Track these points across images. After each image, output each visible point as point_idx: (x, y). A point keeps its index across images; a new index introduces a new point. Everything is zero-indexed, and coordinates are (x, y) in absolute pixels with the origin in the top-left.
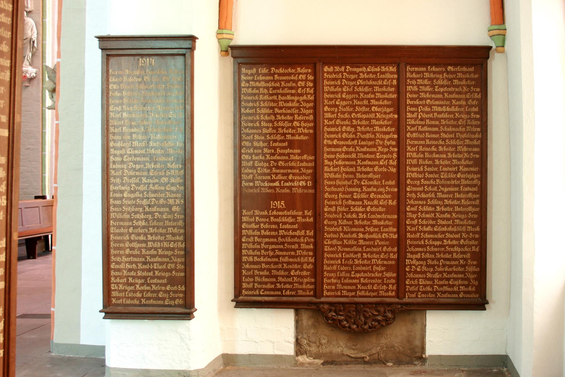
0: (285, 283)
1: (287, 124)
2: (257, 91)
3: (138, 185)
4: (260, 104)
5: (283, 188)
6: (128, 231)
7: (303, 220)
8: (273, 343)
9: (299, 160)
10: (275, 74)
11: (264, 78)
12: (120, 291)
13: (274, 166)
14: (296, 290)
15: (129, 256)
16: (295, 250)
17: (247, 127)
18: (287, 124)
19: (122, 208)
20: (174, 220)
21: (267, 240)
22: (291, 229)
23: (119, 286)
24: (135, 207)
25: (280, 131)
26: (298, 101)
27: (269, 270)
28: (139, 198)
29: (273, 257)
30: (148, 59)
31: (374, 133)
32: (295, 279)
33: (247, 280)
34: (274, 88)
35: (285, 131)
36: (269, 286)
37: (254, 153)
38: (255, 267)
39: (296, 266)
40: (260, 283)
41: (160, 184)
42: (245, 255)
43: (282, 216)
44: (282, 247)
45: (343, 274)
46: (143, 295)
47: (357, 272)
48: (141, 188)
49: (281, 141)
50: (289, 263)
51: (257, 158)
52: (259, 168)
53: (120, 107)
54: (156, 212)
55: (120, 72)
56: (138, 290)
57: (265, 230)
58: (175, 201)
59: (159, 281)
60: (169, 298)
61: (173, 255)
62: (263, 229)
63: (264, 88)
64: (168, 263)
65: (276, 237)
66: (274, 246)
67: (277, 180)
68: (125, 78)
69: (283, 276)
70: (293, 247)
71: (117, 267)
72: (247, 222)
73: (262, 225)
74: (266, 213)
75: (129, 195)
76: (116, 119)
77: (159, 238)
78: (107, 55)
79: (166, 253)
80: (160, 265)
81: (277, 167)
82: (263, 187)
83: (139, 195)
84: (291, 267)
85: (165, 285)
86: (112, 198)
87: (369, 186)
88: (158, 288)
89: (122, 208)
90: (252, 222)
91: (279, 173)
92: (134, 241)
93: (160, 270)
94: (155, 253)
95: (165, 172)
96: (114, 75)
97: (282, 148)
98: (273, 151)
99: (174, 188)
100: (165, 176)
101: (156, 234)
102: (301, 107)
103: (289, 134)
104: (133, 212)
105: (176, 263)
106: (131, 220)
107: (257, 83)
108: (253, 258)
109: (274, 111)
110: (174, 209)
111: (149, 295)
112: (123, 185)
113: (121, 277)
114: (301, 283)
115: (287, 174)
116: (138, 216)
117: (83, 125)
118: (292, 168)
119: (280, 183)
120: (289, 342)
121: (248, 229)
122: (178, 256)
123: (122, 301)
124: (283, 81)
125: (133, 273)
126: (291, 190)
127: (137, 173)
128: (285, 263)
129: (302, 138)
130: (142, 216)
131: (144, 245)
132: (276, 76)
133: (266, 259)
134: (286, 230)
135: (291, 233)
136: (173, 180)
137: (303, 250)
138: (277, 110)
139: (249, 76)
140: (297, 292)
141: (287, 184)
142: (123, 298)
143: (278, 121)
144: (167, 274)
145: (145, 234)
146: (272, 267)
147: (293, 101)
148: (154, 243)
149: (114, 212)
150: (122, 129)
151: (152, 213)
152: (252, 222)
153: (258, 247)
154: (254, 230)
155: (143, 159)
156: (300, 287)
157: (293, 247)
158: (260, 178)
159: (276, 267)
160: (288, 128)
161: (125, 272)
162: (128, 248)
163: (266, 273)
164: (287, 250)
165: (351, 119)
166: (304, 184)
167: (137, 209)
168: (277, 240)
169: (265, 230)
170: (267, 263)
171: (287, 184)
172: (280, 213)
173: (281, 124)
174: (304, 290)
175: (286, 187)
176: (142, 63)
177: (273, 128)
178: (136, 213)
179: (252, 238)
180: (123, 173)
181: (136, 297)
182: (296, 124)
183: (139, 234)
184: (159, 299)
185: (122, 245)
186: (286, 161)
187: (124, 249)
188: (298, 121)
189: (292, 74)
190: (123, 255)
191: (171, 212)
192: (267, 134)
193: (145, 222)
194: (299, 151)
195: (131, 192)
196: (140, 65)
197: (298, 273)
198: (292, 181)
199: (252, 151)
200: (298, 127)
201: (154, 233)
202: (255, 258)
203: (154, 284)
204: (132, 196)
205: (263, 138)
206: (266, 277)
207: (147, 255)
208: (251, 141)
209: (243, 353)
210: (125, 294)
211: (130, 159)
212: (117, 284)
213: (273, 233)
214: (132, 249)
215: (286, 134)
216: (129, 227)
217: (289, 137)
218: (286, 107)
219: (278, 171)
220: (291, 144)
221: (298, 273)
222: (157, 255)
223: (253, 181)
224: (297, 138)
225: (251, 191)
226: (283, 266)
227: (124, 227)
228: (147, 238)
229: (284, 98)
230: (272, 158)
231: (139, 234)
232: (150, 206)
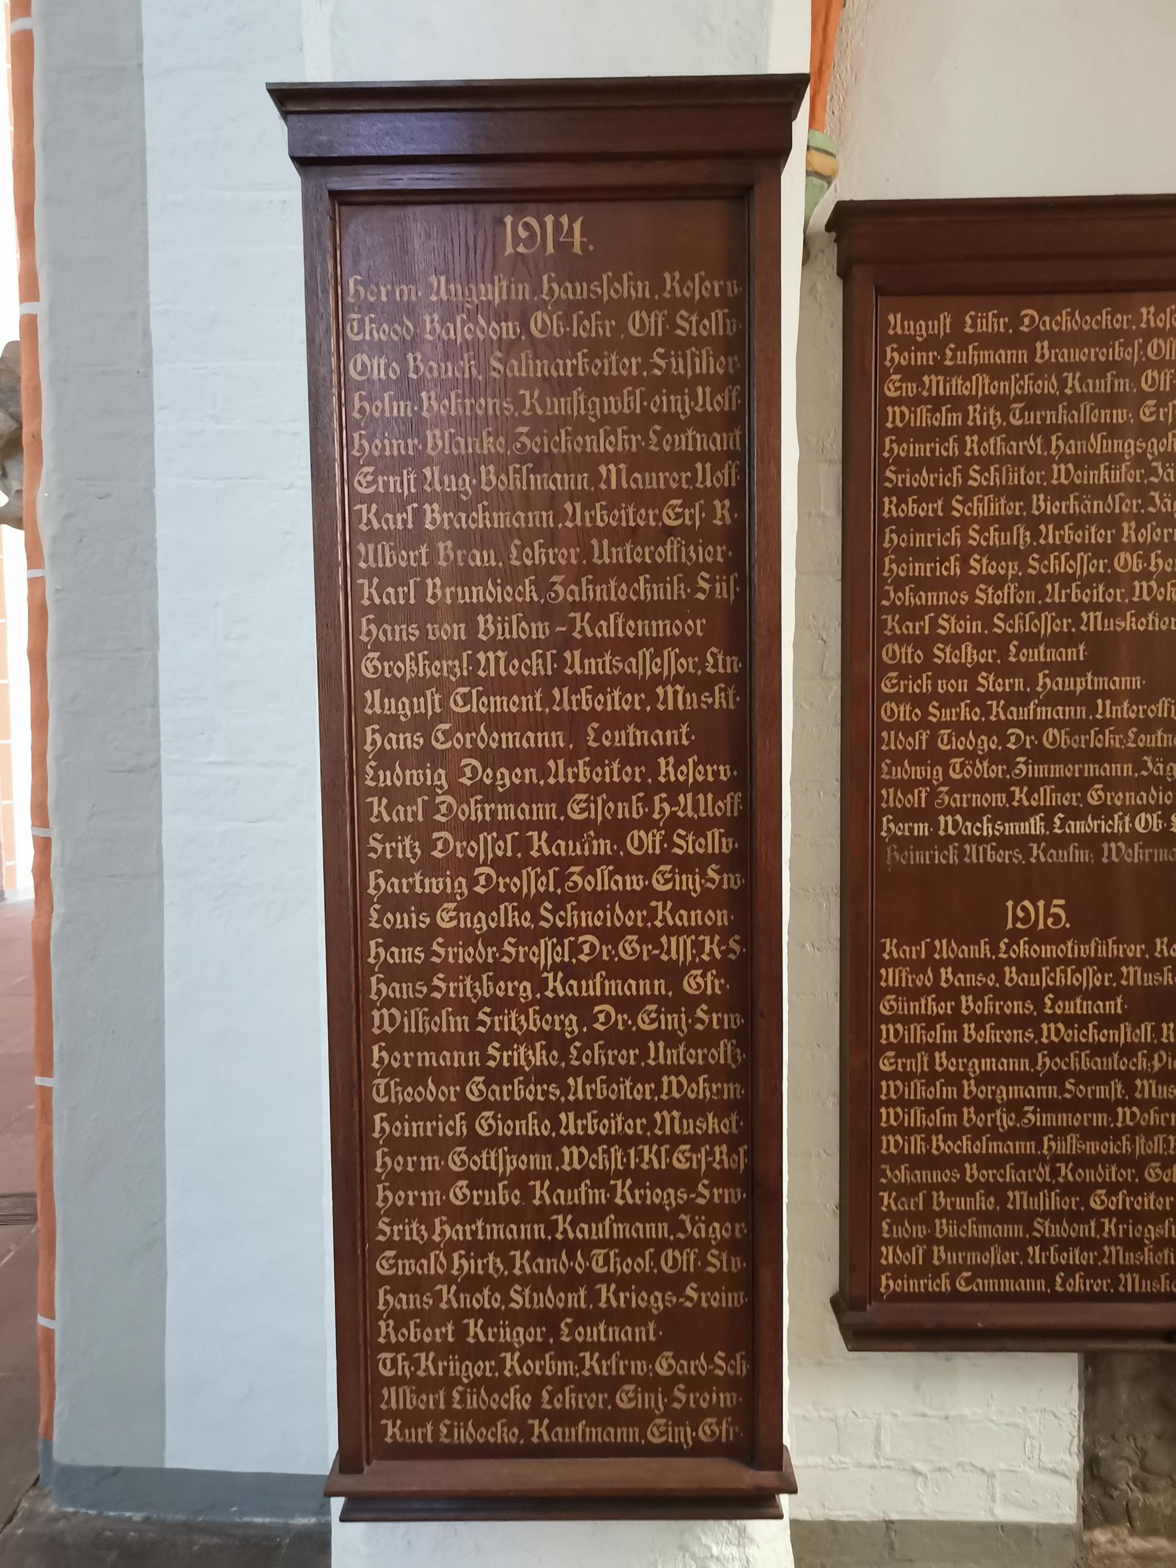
0: (1065, 1244)
1: (1083, 565)
2: (955, 419)
4: (966, 477)
5: (1059, 842)
6: (461, 1095)
7: (1149, 980)
8: (991, 1475)
9: (1137, 722)
10: (1036, 334)
11: (986, 357)
12: (423, 1386)
13: (1022, 751)
14: (1112, 1272)
15: (467, 1214)
16: (1108, 1107)
17: (909, 579)
18: (1083, 565)
19: (428, 983)
20: (696, 1040)
21: (988, 1064)
22: (1093, 1017)
23: (416, 1363)
24: (494, 980)
25: (1056, 594)
26: (1140, 461)
27: (997, 1190)
28: (515, 931)
29: (1013, 1134)
30: (549, 220)
32: (1109, 1225)
33: (900, 1233)
34: (1033, 403)
35: (1076, 595)
36: (994, 1257)
37: (934, 695)
38: (937, 1177)
39: (1112, 1174)
40: (952, 1244)
41: (623, 864)
42: (891, 1130)
43: (1055, 962)
44: (1052, 1092)
46: (536, 1401)
48: (530, 882)
49: (1055, 641)
50: (1081, 1161)
51: (948, 715)
52: (957, 761)
53: (409, 475)
54: (603, 999)
55: (404, 292)
56: (515, 1379)
57: (980, 1021)
58: (698, 946)
59: (616, 1334)
60: (668, 1413)
61: (690, 1207)
62: (972, 1017)
63: (987, 401)
64: (661, 1245)
65: (1028, 1051)
66: (1016, 1092)
67: (1033, 811)
68: (431, 323)
69: (1055, 1217)
70: (1102, 1092)
71: (408, 1267)
72: (899, 992)
73: (966, 1001)
74: (983, 950)
75: (465, 920)
76: (388, 535)
77: (617, 1124)
78: (333, 194)
79: (655, 1197)
80: (622, 1256)
81: (1038, 755)
82: (972, 839)
83: (514, 920)
84: (1089, 1175)
85: (649, 1352)
86: (374, 934)
88: (616, 1365)
89: (428, 983)
90: (925, 991)
91: (1045, 781)
92: (494, 1142)
93: (623, 1283)
94: (599, 1196)
95: (648, 802)
96: (371, 307)
98: (1019, 684)
99: (691, 883)
100: (647, 823)
101: (605, 1108)
102: (1154, 487)
103: (1092, 607)
104: (484, 1002)
105: (703, 1245)
106: (473, 1041)
107: (957, 381)
108: (928, 1141)
109: (1028, 506)
110: (690, 984)
111: (569, 1399)
112: (431, 868)
113: (428, 1319)
114: (1136, 1245)
115: (1082, 785)
116: (510, 1021)
117: (153, 584)
118: (1102, 756)
119: (1049, 825)
120: (1055, 1472)
121: (906, 1020)
122: (712, 1212)
123: (436, 1432)
124: (1071, 367)
125: (485, 1299)
126: (1099, 853)
127: (506, 812)
128: (1066, 1159)
130: (533, 1022)
131: (540, 1161)
132: (1043, 348)
133: (986, 1146)
134: (1069, 1020)
135: (1091, 1034)
136: (685, 844)
137: (1145, 1105)
138: (1040, 503)
139: (921, 347)
140: (1116, 1282)
141: (1078, 827)
142: (436, 1416)
143: (1044, 552)
145: (549, 1110)
146: (1010, 1175)
147: (1114, 459)
148: (592, 1150)
149: (388, 1003)
150: (421, 589)
151: (583, 1007)
152: (925, 991)
153: (950, 1092)
154: (930, 1022)
155: (532, 740)
156: (1131, 1259)
157: (1102, 1092)
158: (960, 800)
159: (1025, 1176)
160: (1088, 582)
161: (447, 1293)
162: (460, 1176)
163: (982, 1202)
164: (1075, 1106)
166: (1156, 824)
167: (504, 989)
168: (1033, 1063)
169: (980, 1021)
170: (985, 1161)
171: (1078, 827)
172: (1048, 951)
173: (1057, 564)
174: (1147, 1272)
175: (1076, 837)
176: (516, 239)
177: (1024, 582)
178: (499, 1005)
179: (923, 1057)
180: (431, 808)
181: (501, 1413)
182: (1126, 561)
183: (514, 1110)
184: (616, 1417)
185: (430, 1163)
186: (1076, 727)
188: (1134, 548)
189: (1114, 334)
190: (436, 1211)
191: (678, 1001)
192: (994, 609)
193: (548, 1049)
194: (1137, 683)
195: (473, 903)
196: (509, 250)
197: (1121, 1200)
198: (1104, 812)
199: (926, 685)
200: (1134, 576)
201: (595, 1103)
202: (937, 1140)
203: (592, 1347)
204: (481, 922)
205: (976, 627)
206: (984, 1217)
207: (558, 1209)
208: (923, 643)
209: (864, 1517)
210: (449, 1400)
211: (465, 739)
212: (410, 1349)
213: (1015, 1036)
214: (483, 1180)
215: (1081, 606)
216: (465, 1075)
217: (1093, 621)
218: (1082, 488)
219: (1041, 771)
220: (1103, 654)
221: (1121, 1200)
222: (610, 1207)
223: (929, 814)
224: (1129, 623)
225: (921, 857)
226: (1055, 1172)
227: (441, 1076)
228: (556, 1125)
229: (1074, 447)
230: (1015, 714)
231: (514, 1110)
232: (571, 971)
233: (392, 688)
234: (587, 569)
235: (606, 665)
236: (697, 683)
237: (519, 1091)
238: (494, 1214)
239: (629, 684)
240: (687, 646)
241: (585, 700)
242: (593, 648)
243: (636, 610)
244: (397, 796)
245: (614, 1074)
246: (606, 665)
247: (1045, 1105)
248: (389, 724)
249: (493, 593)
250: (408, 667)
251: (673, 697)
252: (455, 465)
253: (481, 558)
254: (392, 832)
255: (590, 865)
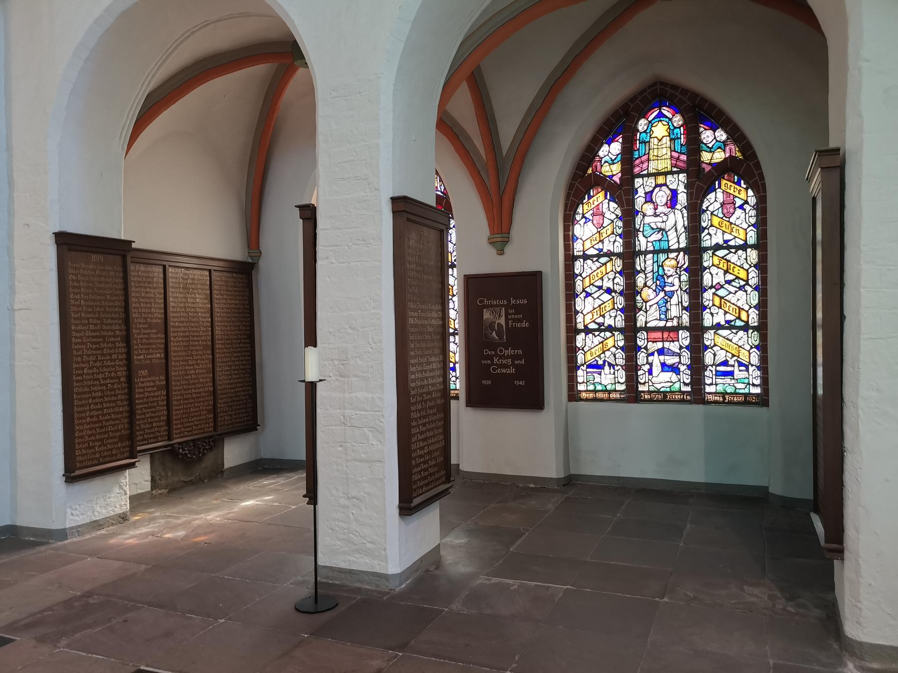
3: (95, 362)
12: (83, 455)
16: (155, 407)
31: (198, 317)
41: (112, 360)
45: (184, 420)
47: (192, 417)
48: (98, 364)
50: (152, 418)
71: (80, 434)
77: (112, 405)
81: (142, 344)
85: (117, 443)
87: (197, 355)
92: (93, 410)
97: (145, 329)
99: (121, 363)
101: (110, 402)
106: (90, 392)
111: (106, 453)
112: (83, 362)
113: (83, 443)
116: (95, 388)
118: (151, 344)
125: (93, 438)
127: (94, 352)
129: (157, 321)
131: (100, 412)
136: (120, 357)
144: (118, 434)
145: (101, 403)
151: (106, 385)
155: (98, 340)
165: (185, 307)
167: (95, 383)
173: (143, 310)
178: (94, 386)
183: (96, 404)
185: (83, 415)
186: (147, 339)
187: (85, 418)
191: (120, 383)
197: (158, 424)
198: (152, 354)
204: (91, 371)
212: (80, 449)
214: (92, 417)
221: (158, 424)
224: (154, 321)
227: (85, 399)
231: (96, 404)
233: (77, 331)
234: (105, 312)
235: (108, 327)
236: (121, 330)
237: (97, 400)
238: (94, 423)
239: (112, 331)
240: (120, 325)
241: (106, 333)
242: (106, 325)
243: (112, 319)
244: (77, 350)
245: (111, 396)
246: (108, 327)
247: (146, 408)
248: (76, 337)
249: (92, 316)
250: (79, 328)
251: (118, 333)
252: (85, 294)
253: (90, 310)
254: (77, 356)
255: (107, 361)
